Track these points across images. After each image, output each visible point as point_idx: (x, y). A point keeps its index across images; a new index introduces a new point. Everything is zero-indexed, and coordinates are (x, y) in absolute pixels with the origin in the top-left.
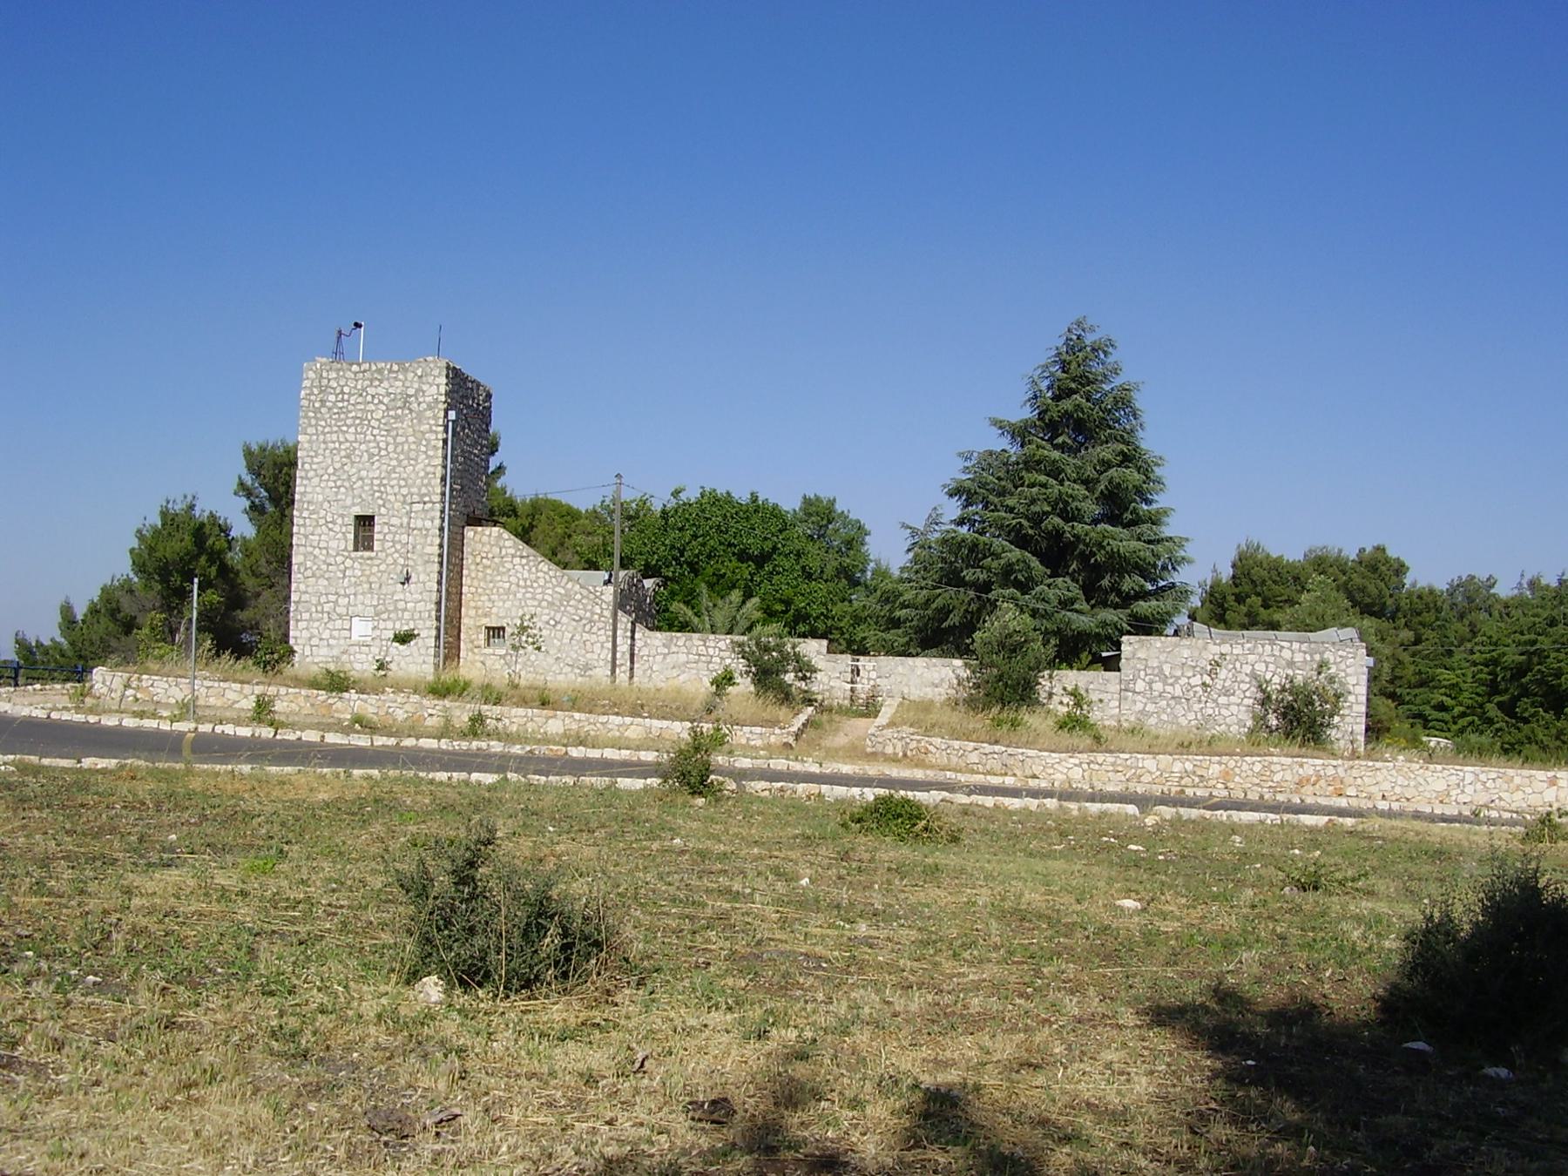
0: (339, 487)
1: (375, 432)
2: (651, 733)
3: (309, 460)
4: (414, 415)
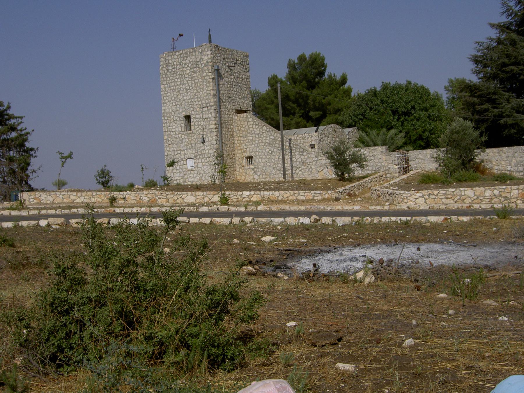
0: (177, 105)
1: (187, 79)
2: (264, 197)
3: (165, 95)
4: (200, 70)
